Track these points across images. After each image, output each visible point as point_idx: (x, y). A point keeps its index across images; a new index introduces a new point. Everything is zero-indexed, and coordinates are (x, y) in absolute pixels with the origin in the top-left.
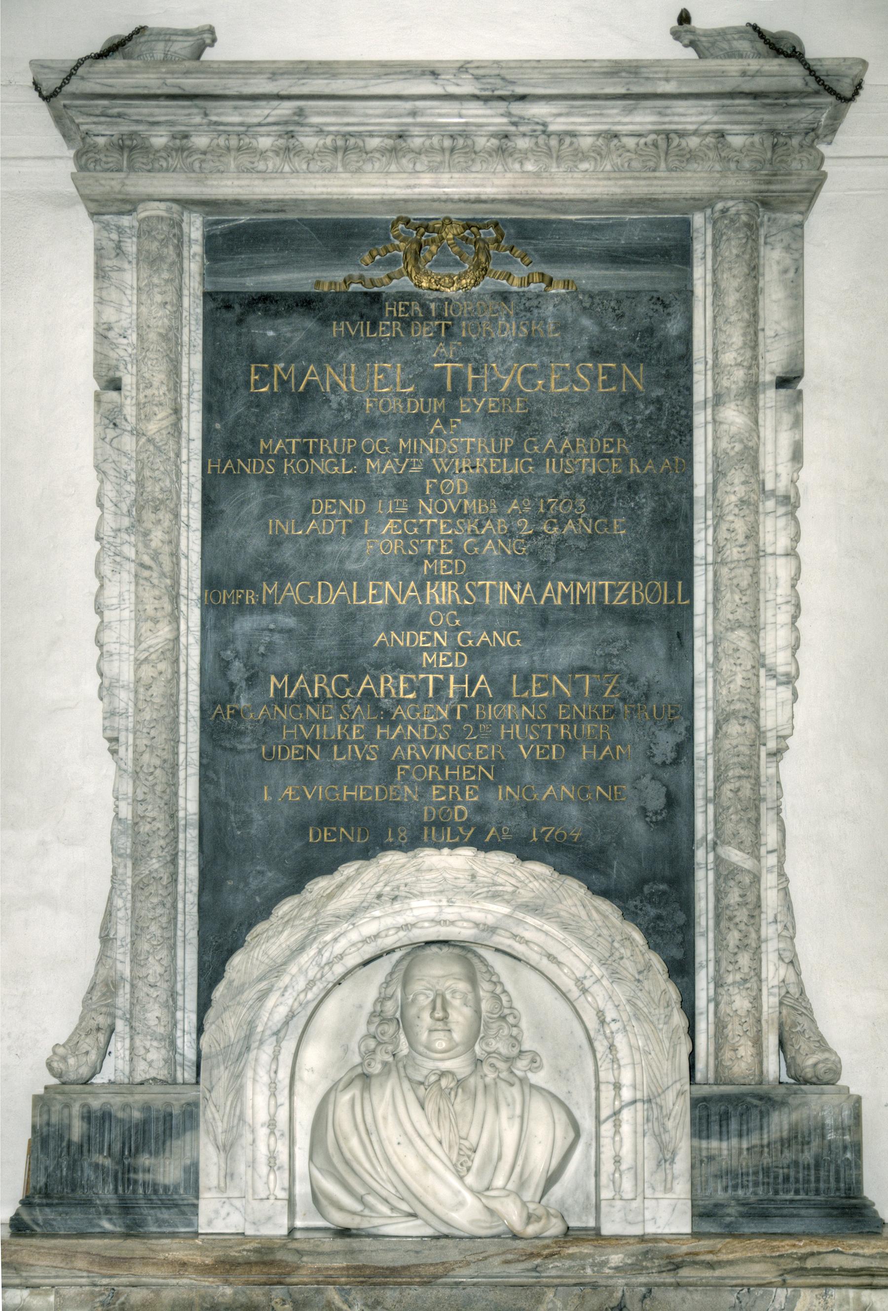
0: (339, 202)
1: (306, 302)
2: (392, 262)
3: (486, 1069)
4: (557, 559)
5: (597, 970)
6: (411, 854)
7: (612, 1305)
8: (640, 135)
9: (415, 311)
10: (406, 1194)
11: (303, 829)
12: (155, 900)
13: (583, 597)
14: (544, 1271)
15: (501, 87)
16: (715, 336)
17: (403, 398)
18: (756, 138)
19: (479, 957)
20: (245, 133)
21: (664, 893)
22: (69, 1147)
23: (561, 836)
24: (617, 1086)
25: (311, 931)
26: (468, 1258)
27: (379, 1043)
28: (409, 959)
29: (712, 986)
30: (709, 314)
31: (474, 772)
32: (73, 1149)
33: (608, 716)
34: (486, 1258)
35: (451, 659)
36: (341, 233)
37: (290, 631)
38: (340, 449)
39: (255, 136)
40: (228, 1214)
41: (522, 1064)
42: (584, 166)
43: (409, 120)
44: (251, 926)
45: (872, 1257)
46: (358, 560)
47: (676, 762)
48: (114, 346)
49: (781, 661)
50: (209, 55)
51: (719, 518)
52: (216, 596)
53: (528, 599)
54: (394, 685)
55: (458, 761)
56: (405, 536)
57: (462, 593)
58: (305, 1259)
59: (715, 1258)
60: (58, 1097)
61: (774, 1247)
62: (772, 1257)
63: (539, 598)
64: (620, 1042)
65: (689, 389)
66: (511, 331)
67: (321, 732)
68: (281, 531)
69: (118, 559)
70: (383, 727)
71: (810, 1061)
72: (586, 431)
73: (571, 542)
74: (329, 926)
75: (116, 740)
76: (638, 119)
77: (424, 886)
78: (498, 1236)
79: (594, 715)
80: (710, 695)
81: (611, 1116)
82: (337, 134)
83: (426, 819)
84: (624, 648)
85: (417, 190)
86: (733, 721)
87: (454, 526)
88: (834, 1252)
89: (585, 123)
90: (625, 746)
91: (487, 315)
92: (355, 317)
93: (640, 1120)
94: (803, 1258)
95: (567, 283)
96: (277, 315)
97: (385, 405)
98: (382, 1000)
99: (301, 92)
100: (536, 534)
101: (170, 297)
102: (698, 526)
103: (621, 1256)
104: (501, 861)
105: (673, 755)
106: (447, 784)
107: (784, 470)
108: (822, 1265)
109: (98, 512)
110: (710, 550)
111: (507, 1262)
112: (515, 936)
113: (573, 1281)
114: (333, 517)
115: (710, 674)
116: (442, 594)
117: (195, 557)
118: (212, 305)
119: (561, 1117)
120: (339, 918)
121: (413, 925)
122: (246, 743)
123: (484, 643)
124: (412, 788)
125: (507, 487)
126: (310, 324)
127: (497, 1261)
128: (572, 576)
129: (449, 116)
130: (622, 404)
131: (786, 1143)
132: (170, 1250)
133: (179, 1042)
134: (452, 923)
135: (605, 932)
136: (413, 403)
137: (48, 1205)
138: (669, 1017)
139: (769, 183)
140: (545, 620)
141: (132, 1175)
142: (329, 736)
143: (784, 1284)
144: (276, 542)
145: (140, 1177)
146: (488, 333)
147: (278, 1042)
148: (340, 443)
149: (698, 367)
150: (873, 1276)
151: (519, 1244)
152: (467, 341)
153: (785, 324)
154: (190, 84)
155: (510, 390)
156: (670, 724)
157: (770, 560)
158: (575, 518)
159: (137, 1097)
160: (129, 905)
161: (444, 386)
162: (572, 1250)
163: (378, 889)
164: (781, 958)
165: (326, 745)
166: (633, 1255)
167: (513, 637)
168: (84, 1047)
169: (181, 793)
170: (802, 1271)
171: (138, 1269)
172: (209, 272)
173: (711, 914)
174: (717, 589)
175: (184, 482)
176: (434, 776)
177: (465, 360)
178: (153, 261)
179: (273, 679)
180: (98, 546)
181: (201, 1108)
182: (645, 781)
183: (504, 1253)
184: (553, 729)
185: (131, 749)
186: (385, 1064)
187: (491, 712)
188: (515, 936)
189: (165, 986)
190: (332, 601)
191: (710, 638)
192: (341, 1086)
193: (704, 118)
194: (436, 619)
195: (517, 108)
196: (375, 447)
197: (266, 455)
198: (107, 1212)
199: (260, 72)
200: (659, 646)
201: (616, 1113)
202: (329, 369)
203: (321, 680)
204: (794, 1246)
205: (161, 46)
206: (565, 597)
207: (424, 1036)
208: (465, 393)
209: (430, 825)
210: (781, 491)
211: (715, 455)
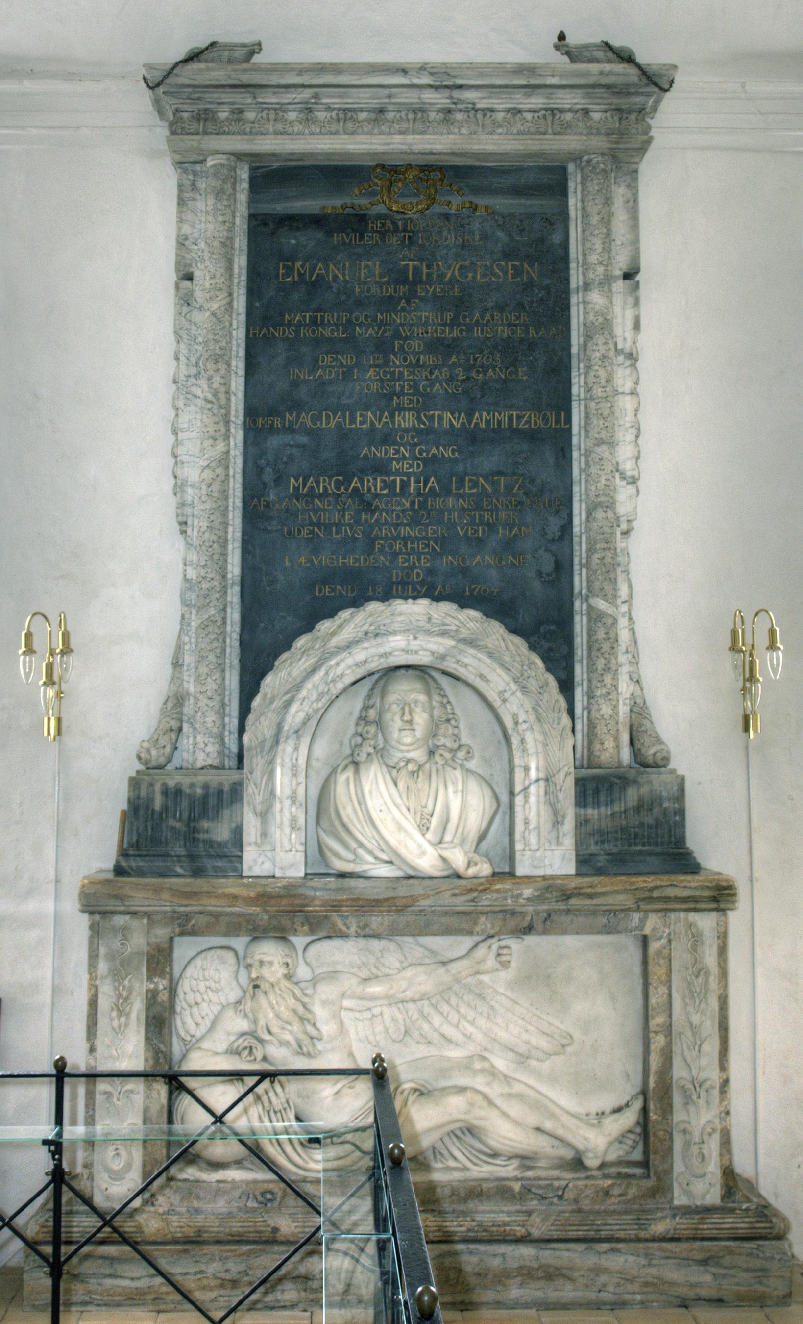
0: (340, 154)
1: (317, 221)
2: (373, 194)
3: (437, 758)
4: (482, 396)
5: (513, 686)
6: (387, 603)
8: (535, 111)
9: (389, 226)
10: (384, 848)
11: (313, 585)
12: (212, 637)
13: (499, 422)
15: (446, 80)
16: (583, 244)
17: (380, 285)
18: (609, 114)
19: (432, 677)
20: (280, 109)
21: (554, 631)
22: (153, 814)
23: (485, 591)
24: (527, 769)
25: (320, 659)
27: (364, 739)
28: (385, 678)
29: (585, 698)
30: (579, 229)
31: (428, 546)
32: (156, 816)
33: (516, 506)
35: (411, 466)
36: (339, 174)
37: (304, 446)
38: (338, 319)
39: (285, 111)
41: (461, 754)
42: (500, 131)
43: (387, 101)
44: (276, 656)
45: (696, 888)
46: (349, 397)
47: (561, 538)
48: (189, 251)
49: (628, 466)
50: (256, 59)
51: (588, 368)
52: (254, 422)
53: (463, 424)
54: (373, 484)
55: (416, 537)
56: (381, 380)
57: (419, 419)
59: (593, 891)
60: (146, 778)
63: (470, 423)
64: (529, 737)
65: (567, 280)
66: (451, 240)
67: (324, 517)
68: (298, 376)
69: (189, 396)
70: (366, 514)
71: (651, 752)
72: (501, 308)
73: (490, 384)
74: (333, 654)
75: (186, 523)
76: (533, 101)
77: (396, 626)
78: (448, 877)
79: (507, 506)
80: (583, 491)
82: (339, 109)
84: (526, 458)
85: (391, 147)
86: (600, 510)
87: (414, 373)
89: (499, 103)
90: (527, 527)
91: (436, 229)
92: (349, 231)
93: (542, 793)
94: (651, 890)
95: (487, 208)
96: (298, 229)
97: (368, 291)
98: (366, 708)
99: (318, 87)
100: (468, 378)
101: (228, 217)
102: (574, 373)
103: (531, 890)
104: (446, 608)
105: (559, 533)
106: (408, 554)
107: (629, 335)
109: (175, 363)
110: (582, 390)
111: (454, 895)
112: (458, 662)
113: (498, 909)
114: (333, 367)
115: (583, 476)
116: (406, 420)
117: (241, 395)
118: (254, 222)
119: (488, 792)
120: (340, 649)
121: (390, 653)
122: (274, 525)
123: (434, 455)
124: (385, 557)
125: (448, 346)
126: (319, 235)
127: (448, 893)
128: (492, 408)
129: (411, 97)
130: (525, 289)
131: (638, 809)
132: (226, 887)
133: (227, 739)
134: (416, 652)
135: (518, 659)
136: (387, 289)
137: (139, 856)
138: (559, 719)
139: (617, 143)
140: (473, 439)
141: (197, 835)
142: (329, 519)
143: (638, 909)
144: (295, 384)
145: (201, 836)
146: (436, 242)
147: (298, 738)
148: (338, 316)
149: (573, 265)
150: (696, 902)
151: (462, 882)
152: (423, 246)
153: (628, 236)
154: (246, 78)
155: (451, 279)
156: (557, 512)
157: (621, 397)
158: (494, 368)
159: (200, 778)
160: (193, 640)
161: (407, 277)
162: (498, 886)
163: (365, 628)
164: (631, 679)
165: (327, 527)
167: (453, 451)
168: (162, 742)
169: (230, 561)
170: (650, 900)
171: (205, 901)
172: (251, 201)
173: (585, 647)
174: (587, 417)
175: (234, 343)
176: (400, 549)
177: (421, 260)
178: (219, 194)
179: (292, 480)
180: (174, 387)
182: (541, 552)
184: (480, 515)
185: (196, 530)
186: (369, 754)
187: (438, 503)
188: (458, 662)
189: (218, 698)
190: (332, 425)
191: (582, 452)
192: (339, 770)
193: (575, 101)
194: (402, 438)
195: (456, 94)
196: (362, 319)
197: (289, 324)
198: (179, 861)
199: (292, 70)
200: (549, 456)
201: (526, 789)
202: (331, 266)
203: (324, 481)
205: (226, 53)
206: (488, 422)
207: (396, 734)
208: (421, 282)
209: (398, 583)
210: (627, 350)
211: (585, 325)
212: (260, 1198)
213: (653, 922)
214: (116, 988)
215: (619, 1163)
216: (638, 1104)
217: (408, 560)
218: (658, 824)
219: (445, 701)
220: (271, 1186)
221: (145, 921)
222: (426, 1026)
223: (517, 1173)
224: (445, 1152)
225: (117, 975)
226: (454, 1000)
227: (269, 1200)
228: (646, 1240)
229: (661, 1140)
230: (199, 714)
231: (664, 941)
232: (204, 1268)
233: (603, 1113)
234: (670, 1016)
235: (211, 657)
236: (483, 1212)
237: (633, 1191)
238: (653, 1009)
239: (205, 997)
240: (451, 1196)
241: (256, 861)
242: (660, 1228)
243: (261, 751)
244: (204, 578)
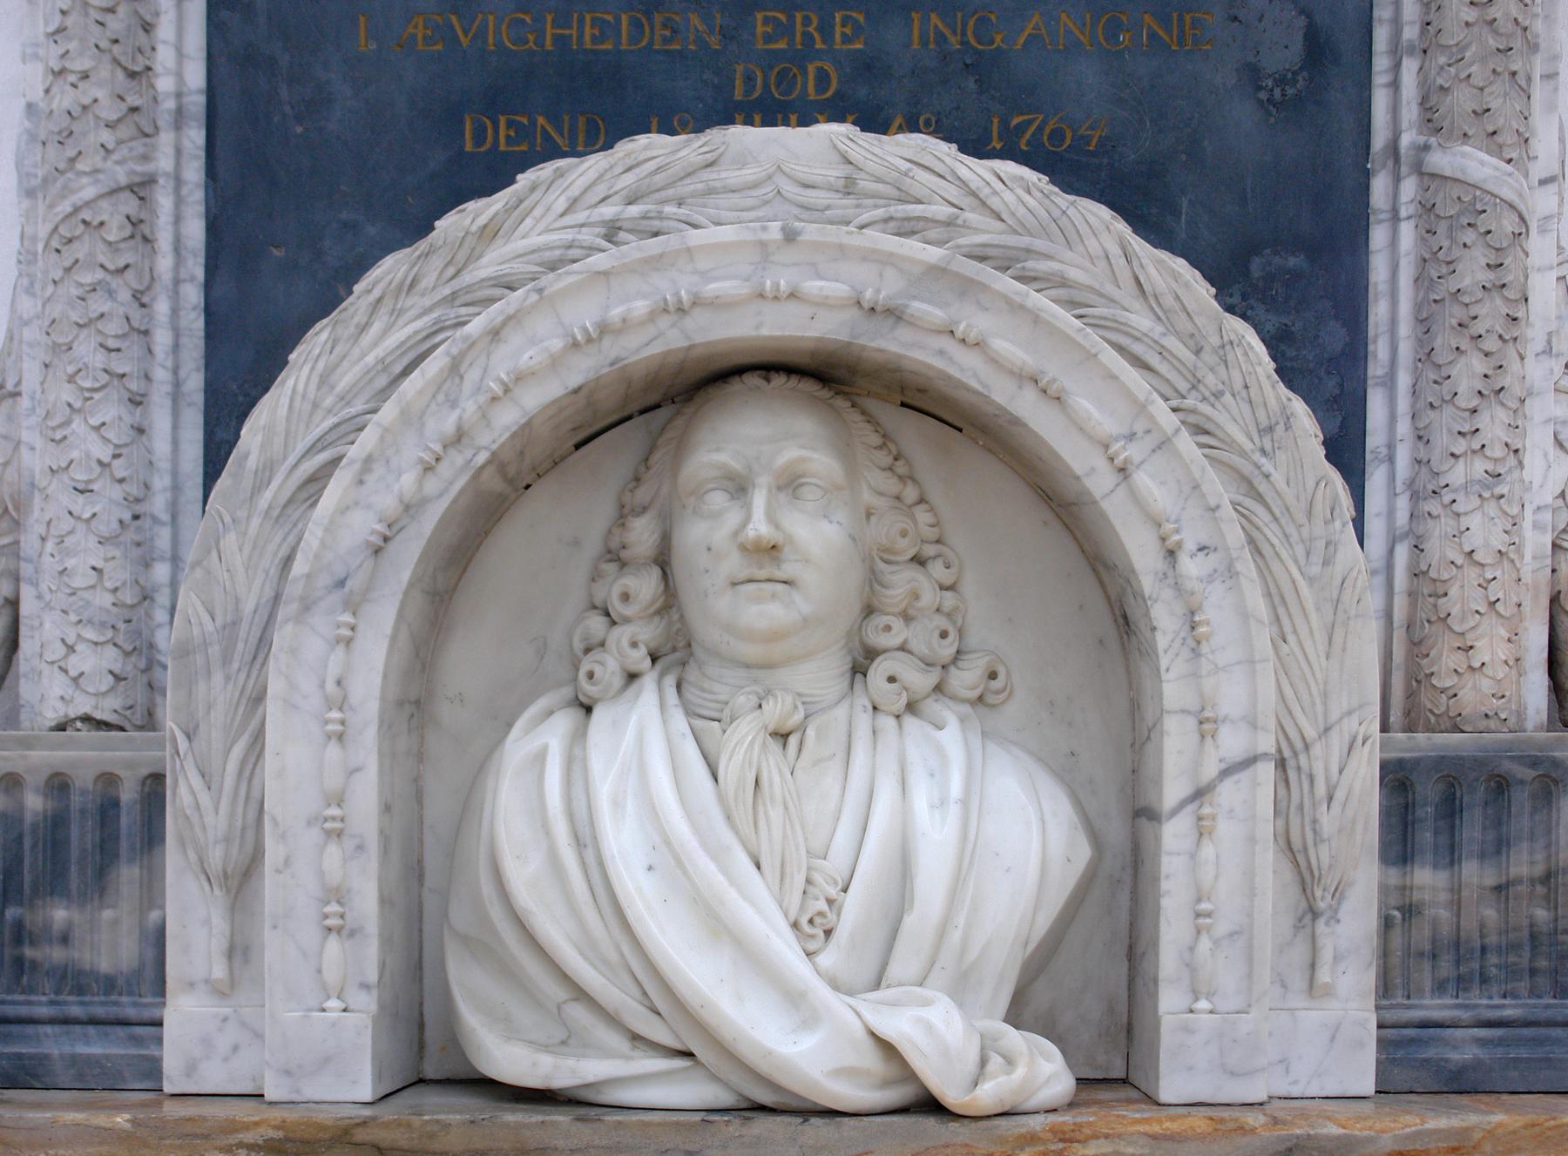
10: (661, 1005)
23: (1057, 135)
29: (1403, 503)
40: (236, 1048)
64: (1217, 611)
81: (1183, 804)
83: (738, 95)
141: (29, 952)
147: (352, 606)
181: (169, 781)
207: (723, 604)
217: (786, 30)
219: (911, 494)
230: (50, 546)
235: (87, 350)
241: (197, 1040)
243: (226, 659)
244: (60, 73)
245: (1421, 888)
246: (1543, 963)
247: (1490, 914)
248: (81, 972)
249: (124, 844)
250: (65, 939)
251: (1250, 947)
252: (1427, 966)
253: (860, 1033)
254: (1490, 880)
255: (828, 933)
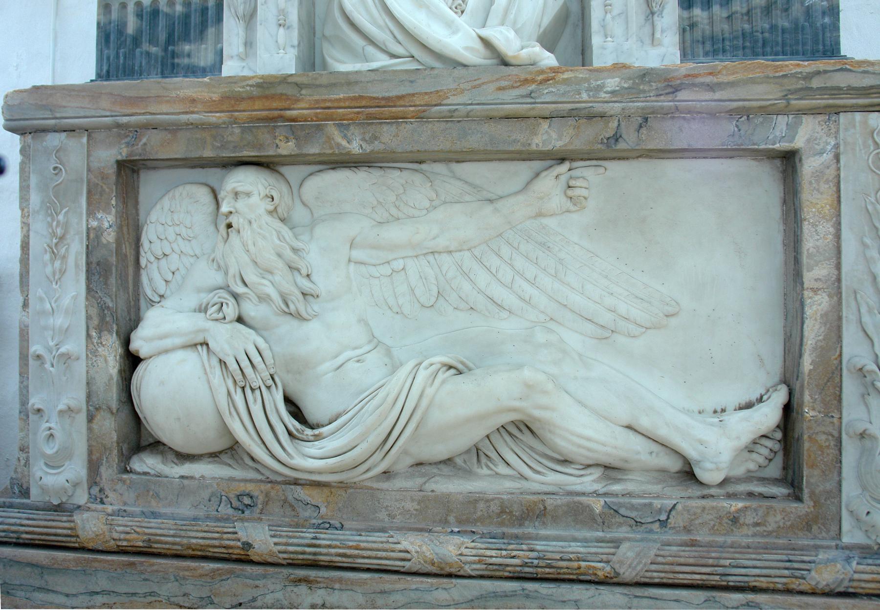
7: (607, 136)
14: (539, 97)
26: (462, 86)
34: (480, 85)
58: (304, 92)
59: (715, 80)
61: (777, 66)
62: (774, 77)
88: (841, 70)
103: (617, 79)
108: (828, 85)
111: (500, 89)
127: (492, 87)
141: (176, 61)
166: (630, 79)
183: (497, 80)
204: (798, 65)
212: (236, 503)
213: (806, 135)
214: (50, 225)
215: (749, 478)
216: (780, 397)
218: (797, 28)
220: (250, 487)
221: (85, 140)
222: (466, 286)
223: (598, 487)
224: (493, 455)
225: (50, 209)
226: (506, 251)
227: (247, 506)
228: (801, 593)
229: (821, 448)
231: (827, 157)
232: (155, 588)
233: (723, 411)
234: (838, 266)
236: (547, 538)
237: (775, 521)
238: (810, 256)
239: (175, 246)
240: (499, 515)
242: (826, 575)
245: (697, 16)
246: (748, 44)
247: (726, 27)
248: (194, 66)
249: (210, 21)
250: (189, 56)
251: (627, 17)
252: (701, 46)
253: (474, 35)
254: (725, 15)
255: (462, 12)
